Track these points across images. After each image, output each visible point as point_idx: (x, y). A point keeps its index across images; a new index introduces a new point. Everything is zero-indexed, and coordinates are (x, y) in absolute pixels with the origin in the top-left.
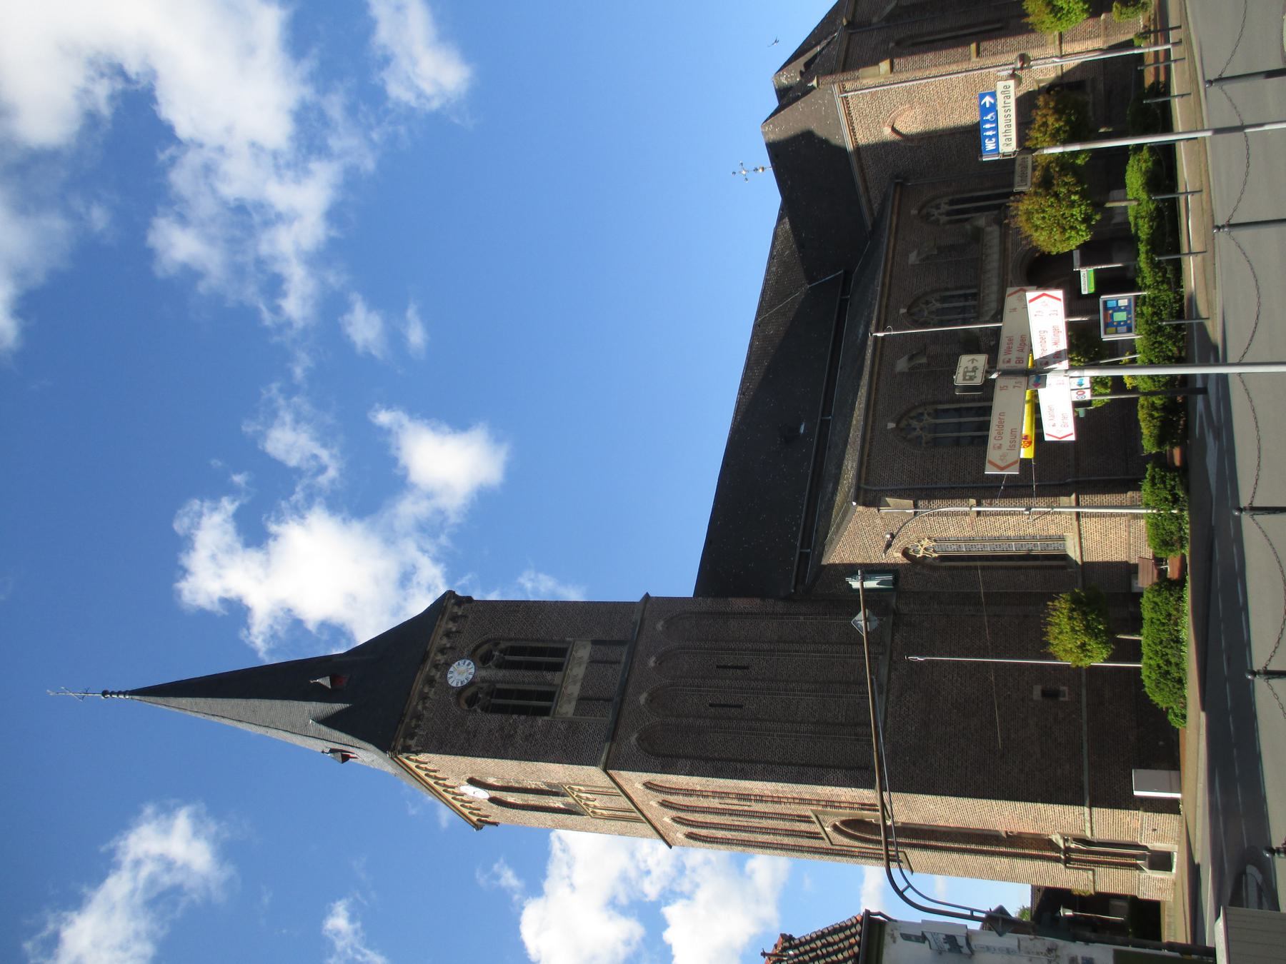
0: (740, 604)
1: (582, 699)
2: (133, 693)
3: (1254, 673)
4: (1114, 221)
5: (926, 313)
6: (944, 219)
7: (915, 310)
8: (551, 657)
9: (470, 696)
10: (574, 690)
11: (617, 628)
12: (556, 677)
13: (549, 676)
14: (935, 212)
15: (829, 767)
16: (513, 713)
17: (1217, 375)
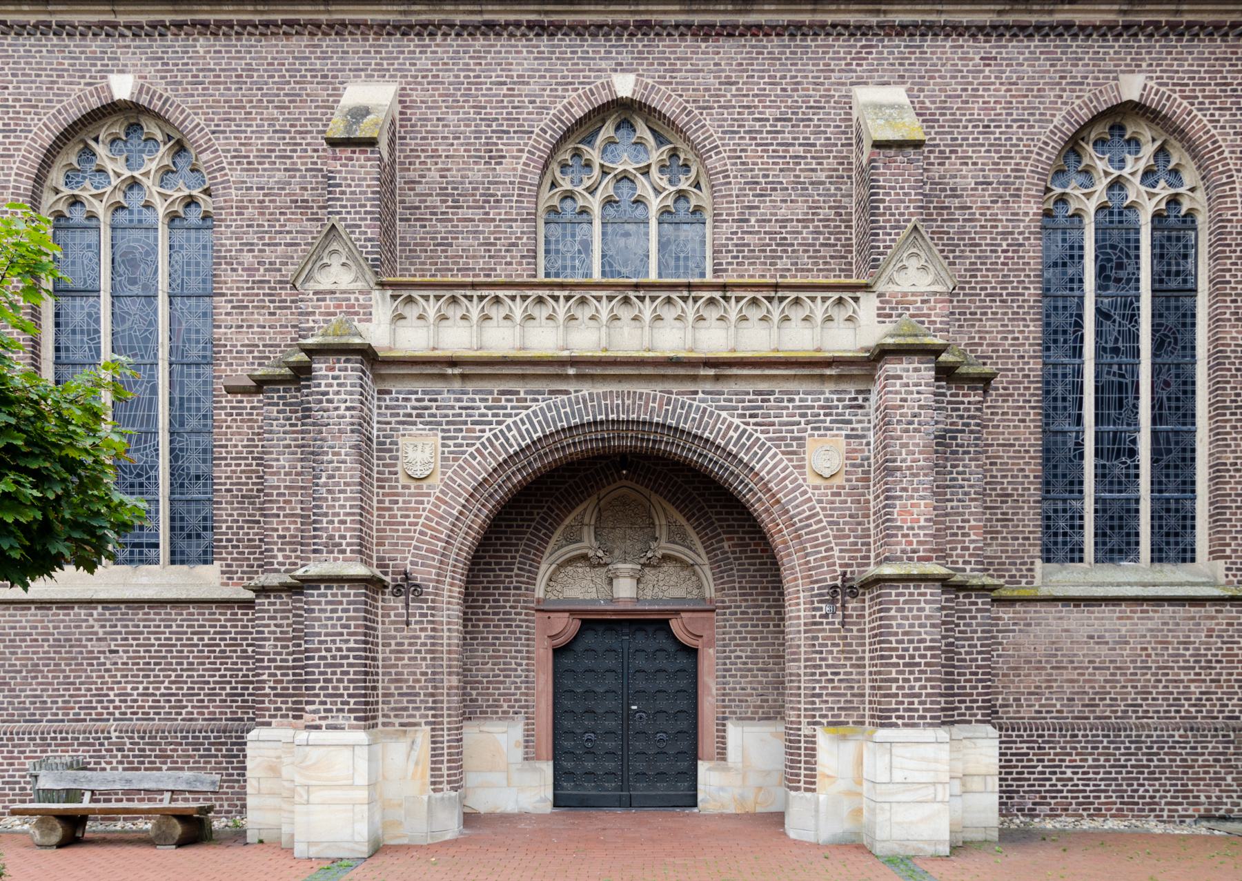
4: (823, 739)
14: (1134, 166)
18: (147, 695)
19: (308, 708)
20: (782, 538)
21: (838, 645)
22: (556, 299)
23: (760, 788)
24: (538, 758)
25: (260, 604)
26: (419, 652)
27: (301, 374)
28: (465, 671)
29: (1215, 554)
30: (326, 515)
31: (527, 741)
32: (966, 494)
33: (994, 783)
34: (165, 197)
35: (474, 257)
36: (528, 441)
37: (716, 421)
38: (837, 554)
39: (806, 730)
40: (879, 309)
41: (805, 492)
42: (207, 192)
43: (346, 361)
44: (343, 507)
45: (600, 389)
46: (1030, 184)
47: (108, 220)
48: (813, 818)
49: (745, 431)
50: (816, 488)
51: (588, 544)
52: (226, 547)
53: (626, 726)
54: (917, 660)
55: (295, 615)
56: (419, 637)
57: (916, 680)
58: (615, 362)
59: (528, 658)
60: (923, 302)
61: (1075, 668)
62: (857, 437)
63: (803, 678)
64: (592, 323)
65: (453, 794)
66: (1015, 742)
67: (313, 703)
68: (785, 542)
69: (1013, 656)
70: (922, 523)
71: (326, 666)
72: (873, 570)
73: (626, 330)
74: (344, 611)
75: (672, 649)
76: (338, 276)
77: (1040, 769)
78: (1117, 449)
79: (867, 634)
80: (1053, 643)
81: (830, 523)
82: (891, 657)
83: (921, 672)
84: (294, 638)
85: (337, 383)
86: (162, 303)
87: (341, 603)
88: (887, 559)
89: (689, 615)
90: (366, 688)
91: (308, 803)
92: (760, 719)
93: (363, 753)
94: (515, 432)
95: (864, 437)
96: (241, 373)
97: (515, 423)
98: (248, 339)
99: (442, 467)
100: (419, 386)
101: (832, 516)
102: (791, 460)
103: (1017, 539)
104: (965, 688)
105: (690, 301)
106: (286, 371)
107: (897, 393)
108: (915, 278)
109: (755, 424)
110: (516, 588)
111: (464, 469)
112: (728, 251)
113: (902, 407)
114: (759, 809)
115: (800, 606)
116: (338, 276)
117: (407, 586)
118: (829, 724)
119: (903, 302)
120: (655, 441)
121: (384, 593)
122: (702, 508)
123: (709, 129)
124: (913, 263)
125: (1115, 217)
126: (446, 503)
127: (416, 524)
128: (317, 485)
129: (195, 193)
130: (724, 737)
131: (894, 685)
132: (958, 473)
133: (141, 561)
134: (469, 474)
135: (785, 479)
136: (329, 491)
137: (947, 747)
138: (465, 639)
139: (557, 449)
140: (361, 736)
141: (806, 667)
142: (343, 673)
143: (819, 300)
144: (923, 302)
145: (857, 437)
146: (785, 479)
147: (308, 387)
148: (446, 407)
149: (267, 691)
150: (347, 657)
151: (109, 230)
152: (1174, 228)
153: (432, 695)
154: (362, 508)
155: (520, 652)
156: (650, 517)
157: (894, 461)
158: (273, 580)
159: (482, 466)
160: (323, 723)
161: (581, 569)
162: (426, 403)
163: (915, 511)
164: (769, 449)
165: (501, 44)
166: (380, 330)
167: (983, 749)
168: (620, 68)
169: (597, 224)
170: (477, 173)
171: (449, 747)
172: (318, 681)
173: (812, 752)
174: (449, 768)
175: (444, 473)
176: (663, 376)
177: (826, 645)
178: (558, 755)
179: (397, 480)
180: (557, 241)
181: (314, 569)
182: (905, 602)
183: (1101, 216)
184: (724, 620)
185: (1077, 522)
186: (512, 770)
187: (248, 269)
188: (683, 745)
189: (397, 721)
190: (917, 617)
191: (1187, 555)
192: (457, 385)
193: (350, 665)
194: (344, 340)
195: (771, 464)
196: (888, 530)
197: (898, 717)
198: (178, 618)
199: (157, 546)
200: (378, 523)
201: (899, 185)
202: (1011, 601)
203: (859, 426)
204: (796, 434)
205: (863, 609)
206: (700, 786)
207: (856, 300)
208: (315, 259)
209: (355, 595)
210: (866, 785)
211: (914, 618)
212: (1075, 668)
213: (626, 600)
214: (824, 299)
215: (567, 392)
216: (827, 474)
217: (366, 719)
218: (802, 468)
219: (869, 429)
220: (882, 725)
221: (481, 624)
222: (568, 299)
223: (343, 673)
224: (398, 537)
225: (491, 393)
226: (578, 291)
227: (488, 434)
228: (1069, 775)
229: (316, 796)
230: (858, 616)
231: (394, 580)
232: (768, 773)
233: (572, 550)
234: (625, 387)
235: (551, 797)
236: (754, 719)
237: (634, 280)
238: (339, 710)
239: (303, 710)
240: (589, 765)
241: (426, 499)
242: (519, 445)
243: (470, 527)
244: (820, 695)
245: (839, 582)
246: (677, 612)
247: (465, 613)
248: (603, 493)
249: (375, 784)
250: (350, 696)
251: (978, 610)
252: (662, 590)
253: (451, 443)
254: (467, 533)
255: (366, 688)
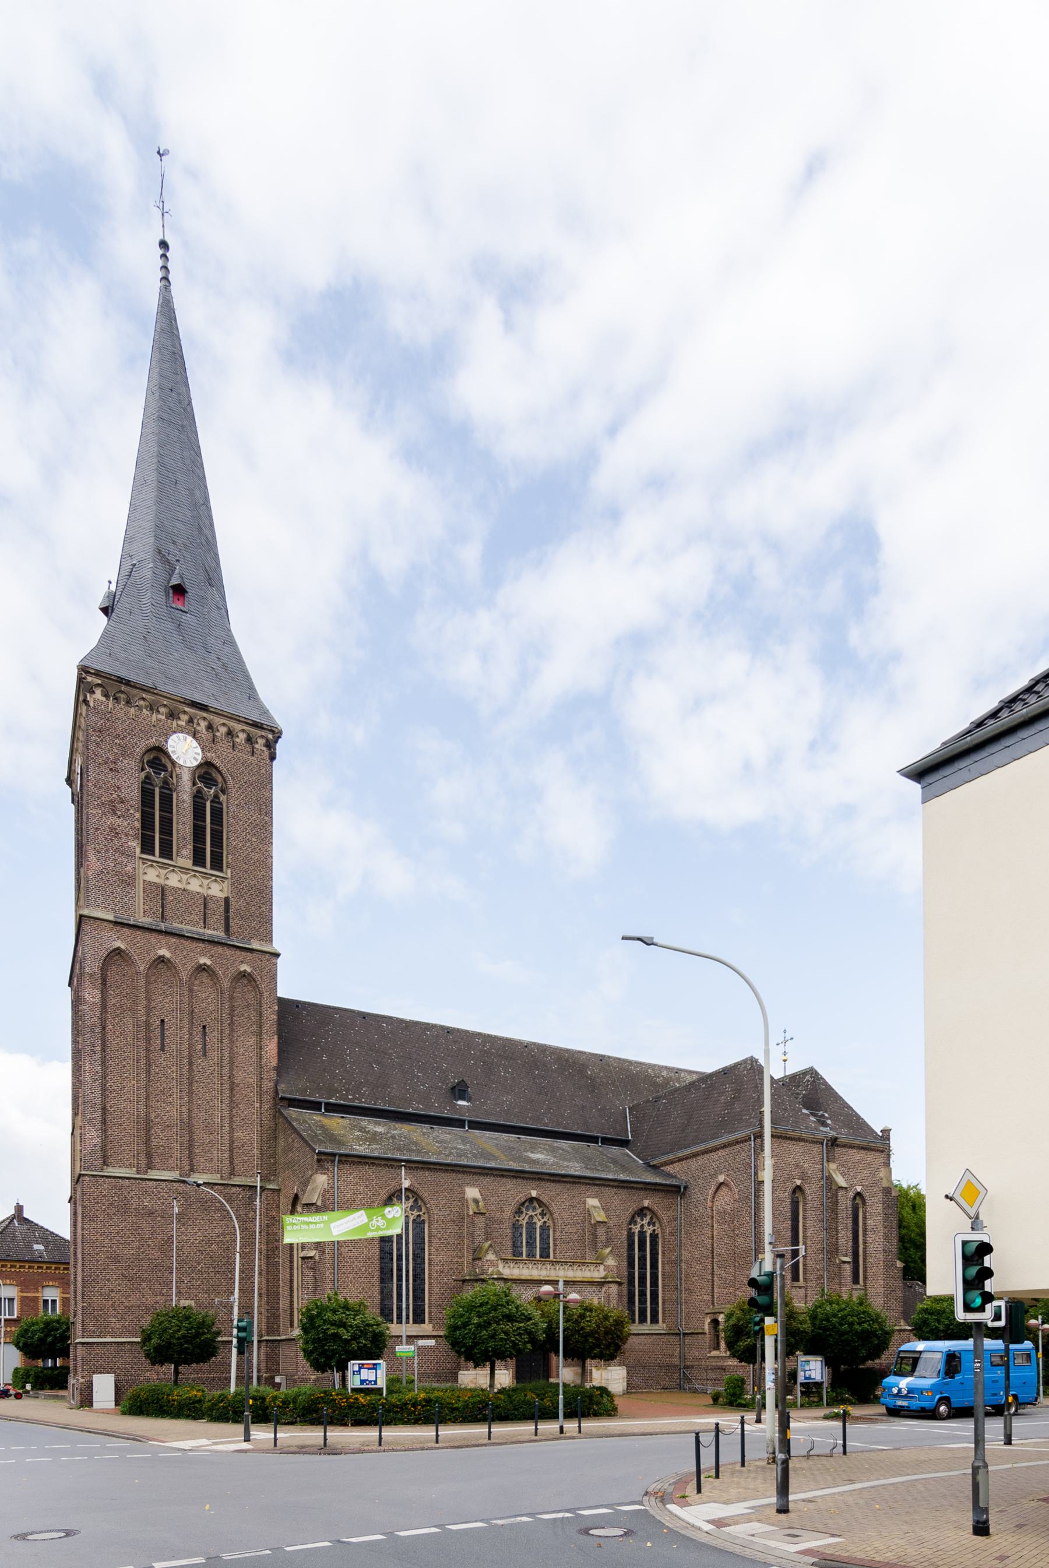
0: (271, 1047)
1: (163, 890)
2: (167, 310)
3: (492, 1385)
4: (594, 1370)
5: (531, 1213)
6: (636, 1229)
7: (535, 1204)
8: (209, 852)
9: (158, 759)
10: (174, 881)
11: (244, 923)
12: (184, 858)
13: (188, 851)
14: (645, 1221)
15: (104, 1131)
16: (143, 813)
17: (564, 1406)
29: (664, 1322)
46: (625, 1226)
78: (642, 1294)
119: (609, 1266)
123: (554, 1207)
125: (642, 1234)
152: (654, 1237)
165: (504, 1180)
168: (533, 1189)
170: (498, 1215)
191: (423, 1322)
201: (601, 1233)
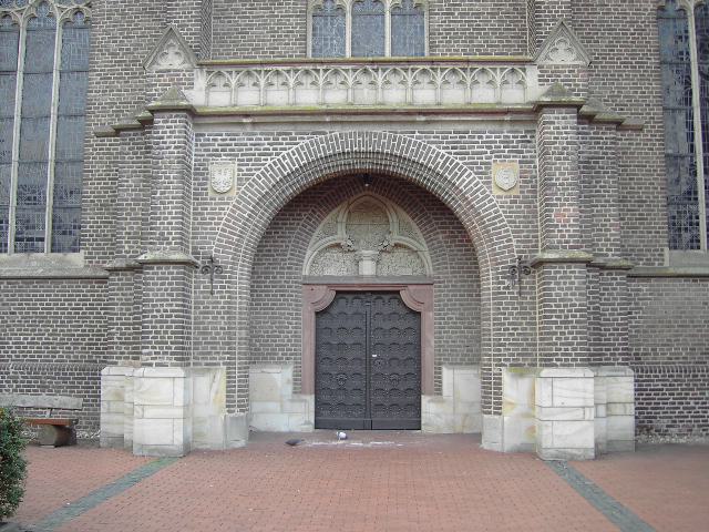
4: (506, 377)
18: (34, 343)
19: (144, 351)
20: (475, 229)
21: (516, 309)
22: (318, 71)
23: (467, 415)
24: (303, 392)
25: (112, 280)
26: (219, 313)
27: (146, 124)
28: (251, 328)
30: (159, 219)
31: (295, 380)
32: (606, 201)
33: (631, 409)
34: (62, 10)
35: (263, 41)
36: (297, 166)
37: (429, 153)
38: (514, 243)
39: (495, 370)
40: (540, 76)
41: (491, 200)
42: (89, 5)
43: (176, 117)
44: (170, 213)
45: (349, 130)
47: (25, 25)
48: (502, 433)
49: (448, 158)
50: (499, 197)
51: (341, 236)
52: (89, 240)
53: (368, 374)
54: (570, 319)
55: (136, 288)
56: (218, 303)
57: (570, 333)
58: (356, 113)
59: (297, 319)
60: (570, 72)
61: (696, 326)
62: (527, 162)
63: (492, 333)
64: (342, 86)
65: (242, 414)
66: (653, 381)
67: (147, 348)
68: (478, 235)
69: (650, 318)
70: (572, 222)
71: (156, 322)
72: (540, 255)
73: (366, 90)
74: (170, 284)
75: (403, 311)
76: (173, 61)
77: (671, 400)
79: (537, 300)
80: (679, 308)
81: (509, 222)
82: (552, 317)
83: (573, 327)
84: (135, 303)
85: (169, 131)
86: (56, 75)
87: (167, 279)
88: (548, 247)
89: (414, 287)
90: (182, 338)
91: (143, 417)
92: (467, 364)
93: (180, 382)
94: (288, 160)
95: (532, 162)
96: (107, 122)
97: (288, 154)
98: (109, 100)
99: (238, 184)
100: (223, 131)
101: (511, 217)
102: (481, 178)
103: (651, 232)
104: (609, 340)
105: (410, 72)
106: (136, 123)
107: (552, 133)
108: (563, 56)
109: (455, 154)
110: (289, 268)
111: (253, 186)
112: (440, 34)
113: (554, 143)
114: (465, 431)
115: (489, 282)
116: (173, 61)
117: (212, 267)
118: (511, 365)
119: (557, 70)
120: (385, 165)
121: (196, 272)
122: (423, 210)
124: (562, 46)
126: (239, 209)
127: (219, 224)
128: (154, 198)
129: (81, 6)
130: (440, 378)
131: (554, 337)
132: (601, 187)
133: (33, 251)
134: (256, 189)
135: (477, 191)
136: (162, 203)
137: (592, 380)
138: (252, 304)
139: (317, 172)
140: (179, 372)
141: (494, 324)
142: (167, 327)
143: (498, 71)
144: (570, 72)
145: (527, 162)
146: (477, 191)
147: (150, 133)
148: (241, 145)
149: (116, 340)
150: (171, 316)
151: (25, 32)
153: (228, 344)
154: (183, 213)
155: (291, 314)
156: (387, 217)
157: (552, 179)
158: (118, 263)
159: (263, 185)
160: (154, 362)
161: (335, 254)
162: (228, 142)
163: (566, 214)
164: (466, 170)
166: (200, 93)
167: (623, 386)
169: (349, 17)
171: (239, 381)
172: (151, 332)
173: (499, 384)
174: (239, 397)
175: (239, 189)
176: (391, 122)
177: (508, 309)
178: (317, 393)
179: (207, 194)
180: (321, 29)
181: (149, 256)
182: (561, 278)
183: (698, 11)
184: (439, 291)
185: (695, 221)
186: (285, 404)
187: (112, 54)
188: (411, 384)
189: (204, 362)
190: (568, 288)
192: (249, 129)
193: (173, 322)
194: (176, 103)
195: (467, 181)
196: (548, 228)
197: (557, 360)
198: (55, 289)
199: (42, 240)
200: (193, 223)
202: (648, 277)
203: (528, 154)
204: (484, 160)
205: (534, 283)
206: (423, 415)
207: (524, 70)
208: (158, 50)
209: (177, 273)
210: (537, 409)
211: (568, 289)
212: (696, 326)
213: (367, 277)
214: (502, 70)
215: (324, 133)
216: (506, 187)
217: (183, 359)
218: (489, 183)
219: (535, 157)
220: (546, 366)
221: (263, 294)
222: (325, 71)
223: (167, 327)
224: (207, 233)
225: (272, 134)
226: (334, 65)
227: (269, 162)
228: (692, 404)
229: (149, 412)
230: (531, 288)
231: (203, 262)
232: (472, 404)
233: (331, 240)
234: (365, 129)
235: (313, 421)
236: (461, 364)
237: (370, 59)
238: (164, 353)
239: (141, 353)
240: (341, 398)
241: (226, 207)
242: (291, 169)
243: (256, 226)
244: (504, 345)
245: (516, 264)
246: (406, 285)
247: (252, 286)
248: (352, 199)
249: (188, 405)
250: (172, 343)
251: (618, 284)
252: (397, 269)
253: (244, 168)
254: (254, 230)
255: (182, 338)
